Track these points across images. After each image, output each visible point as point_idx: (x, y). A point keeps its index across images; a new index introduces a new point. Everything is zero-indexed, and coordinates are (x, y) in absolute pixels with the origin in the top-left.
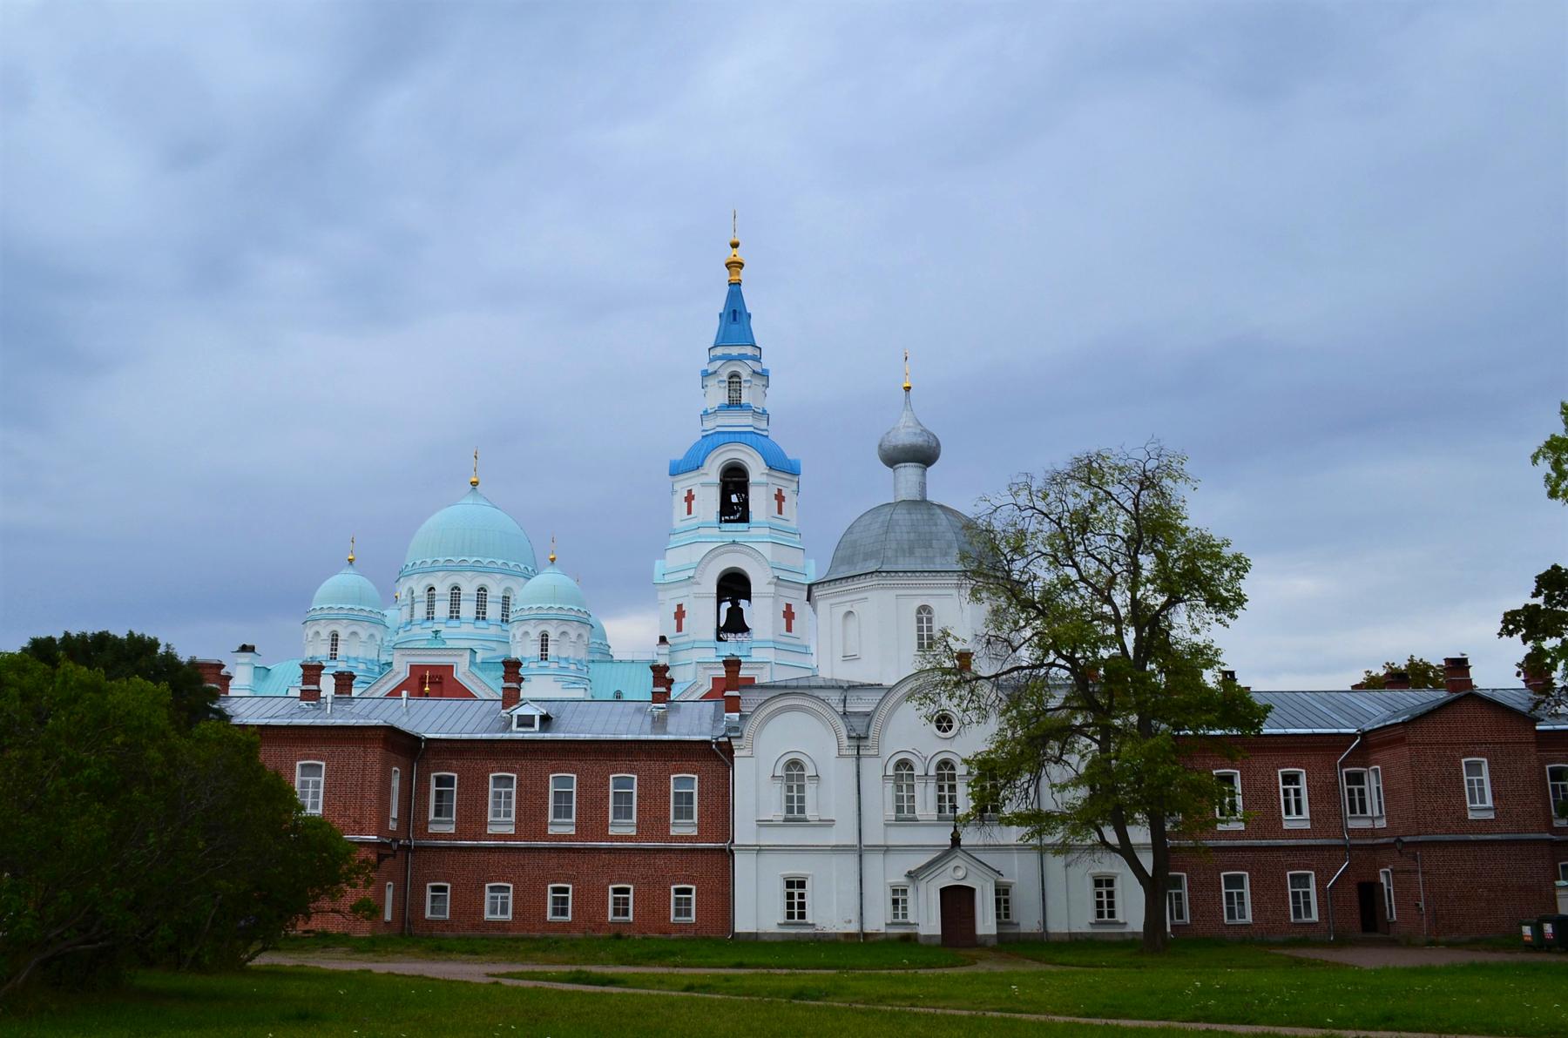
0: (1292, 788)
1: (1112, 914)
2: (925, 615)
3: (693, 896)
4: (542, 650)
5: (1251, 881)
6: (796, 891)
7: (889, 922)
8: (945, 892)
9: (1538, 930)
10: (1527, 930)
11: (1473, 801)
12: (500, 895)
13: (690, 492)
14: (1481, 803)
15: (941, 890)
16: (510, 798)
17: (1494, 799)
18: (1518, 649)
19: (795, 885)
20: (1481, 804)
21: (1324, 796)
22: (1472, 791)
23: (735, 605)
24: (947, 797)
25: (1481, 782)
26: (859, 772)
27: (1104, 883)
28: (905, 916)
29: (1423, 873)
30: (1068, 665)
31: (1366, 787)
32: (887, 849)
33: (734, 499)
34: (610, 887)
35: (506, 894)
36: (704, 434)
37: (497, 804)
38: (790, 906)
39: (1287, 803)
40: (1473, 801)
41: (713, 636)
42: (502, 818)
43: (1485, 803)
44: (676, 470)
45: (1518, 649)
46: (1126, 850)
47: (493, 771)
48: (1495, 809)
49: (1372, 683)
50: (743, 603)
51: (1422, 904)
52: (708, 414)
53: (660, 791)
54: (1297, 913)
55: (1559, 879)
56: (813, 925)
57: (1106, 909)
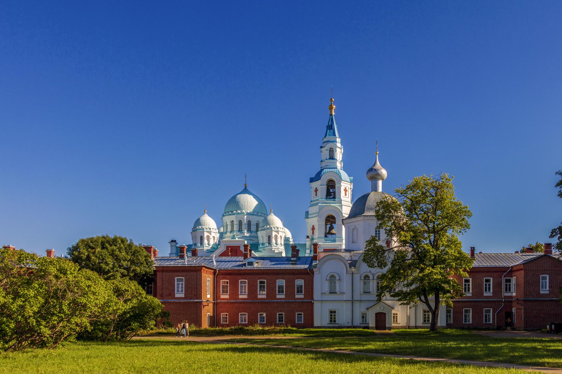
1: (397, 321)
3: (303, 316)
5: (472, 311)
6: (333, 314)
7: (361, 323)
8: (377, 314)
10: (548, 327)
11: (542, 288)
12: (244, 316)
13: (316, 188)
14: (545, 289)
15: (376, 314)
16: (246, 287)
17: (549, 287)
19: (332, 313)
20: (545, 290)
21: (498, 286)
22: (542, 285)
23: (332, 225)
25: (546, 282)
28: (366, 321)
29: (524, 309)
31: (511, 283)
32: (361, 301)
33: (331, 191)
34: (277, 313)
35: (246, 316)
36: (322, 168)
37: (241, 289)
39: (486, 288)
40: (542, 288)
41: (323, 236)
42: (243, 293)
44: (312, 180)
47: (240, 279)
48: (549, 290)
51: (523, 319)
53: (292, 284)
54: (486, 321)
56: (338, 324)
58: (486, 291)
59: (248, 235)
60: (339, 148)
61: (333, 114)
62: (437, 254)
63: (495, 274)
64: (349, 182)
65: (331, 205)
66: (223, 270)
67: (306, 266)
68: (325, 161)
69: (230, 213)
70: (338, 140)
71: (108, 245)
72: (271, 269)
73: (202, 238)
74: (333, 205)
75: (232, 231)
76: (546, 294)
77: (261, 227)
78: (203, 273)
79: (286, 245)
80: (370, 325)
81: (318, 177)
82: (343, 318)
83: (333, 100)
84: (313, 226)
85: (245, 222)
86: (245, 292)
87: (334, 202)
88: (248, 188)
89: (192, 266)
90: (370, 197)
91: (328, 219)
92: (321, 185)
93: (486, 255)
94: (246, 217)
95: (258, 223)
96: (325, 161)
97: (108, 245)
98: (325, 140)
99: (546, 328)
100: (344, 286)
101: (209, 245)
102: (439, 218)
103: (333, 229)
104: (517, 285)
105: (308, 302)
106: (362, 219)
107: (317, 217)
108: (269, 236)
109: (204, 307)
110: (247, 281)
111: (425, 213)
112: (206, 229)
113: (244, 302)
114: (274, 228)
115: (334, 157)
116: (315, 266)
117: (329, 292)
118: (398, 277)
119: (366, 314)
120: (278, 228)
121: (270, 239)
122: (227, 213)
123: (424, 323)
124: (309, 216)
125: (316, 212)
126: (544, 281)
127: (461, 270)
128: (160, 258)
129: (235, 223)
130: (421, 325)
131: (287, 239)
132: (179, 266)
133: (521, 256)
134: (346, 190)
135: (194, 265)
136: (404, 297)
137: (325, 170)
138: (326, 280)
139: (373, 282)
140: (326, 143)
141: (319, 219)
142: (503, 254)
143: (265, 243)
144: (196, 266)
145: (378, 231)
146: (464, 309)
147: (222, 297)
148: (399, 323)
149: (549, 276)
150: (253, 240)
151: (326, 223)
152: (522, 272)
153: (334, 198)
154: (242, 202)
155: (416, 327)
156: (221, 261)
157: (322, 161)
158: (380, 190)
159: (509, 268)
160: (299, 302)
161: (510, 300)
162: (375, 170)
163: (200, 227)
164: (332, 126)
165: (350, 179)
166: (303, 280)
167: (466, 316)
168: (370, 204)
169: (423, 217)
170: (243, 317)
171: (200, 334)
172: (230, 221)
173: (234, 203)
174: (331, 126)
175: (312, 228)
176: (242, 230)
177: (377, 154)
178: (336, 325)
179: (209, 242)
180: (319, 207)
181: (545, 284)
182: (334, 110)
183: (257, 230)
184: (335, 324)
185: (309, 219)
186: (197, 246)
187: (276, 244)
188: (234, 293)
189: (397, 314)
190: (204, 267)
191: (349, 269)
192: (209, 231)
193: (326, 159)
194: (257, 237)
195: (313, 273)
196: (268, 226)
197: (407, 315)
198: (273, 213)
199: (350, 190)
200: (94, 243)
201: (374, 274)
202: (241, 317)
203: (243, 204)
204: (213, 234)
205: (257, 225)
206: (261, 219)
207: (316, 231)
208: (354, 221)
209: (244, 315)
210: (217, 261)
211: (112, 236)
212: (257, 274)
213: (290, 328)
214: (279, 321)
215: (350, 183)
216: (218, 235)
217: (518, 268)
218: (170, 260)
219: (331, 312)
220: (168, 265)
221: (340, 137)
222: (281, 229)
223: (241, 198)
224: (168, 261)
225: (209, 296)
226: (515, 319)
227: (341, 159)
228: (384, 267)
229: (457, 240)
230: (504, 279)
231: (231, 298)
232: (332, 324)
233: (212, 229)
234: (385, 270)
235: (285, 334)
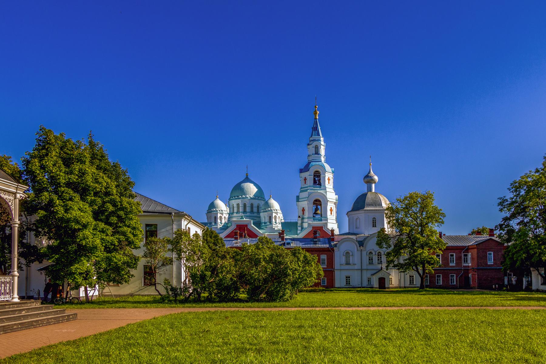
0: (452, 257)
2: (374, 220)
6: (348, 279)
10: (494, 286)
11: (489, 260)
13: (305, 178)
15: (379, 278)
17: (494, 260)
19: (348, 278)
20: (491, 262)
21: (459, 259)
22: (489, 259)
25: (491, 257)
28: (370, 283)
29: (477, 275)
33: (316, 179)
38: (347, 282)
39: (451, 260)
40: (489, 260)
44: (301, 171)
46: (417, 271)
54: (451, 282)
57: (412, 282)
58: (451, 262)
60: (323, 145)
61: (317, 117)
63: (457, 251)
67: (328, 246)
69: (236, 197)
70: (322, 139)
73: (216, 218)
74: (319, 191)
76: (491, 265)
77: (263, 209)
80: (375, 286)
81: (306, 169)
88: (249, 177)
91: (315, 202)
93: (449, 237)
98: (311, 139)
100: (355, 259)
101: (221, 224)
104: (472, 258)
105: (330, 271)
112: (219, 211)
114: (274, 210)
116: (336, 245)
119: (370, 279)
124: (300, 200)
129: (240, 205)
130: (408, 286)
134: (329, 179)
136: (401, 267)
137: (313, 163)
152: (476, 250)
155: (405, 287)
157: (309, 156)
161: (467, 268)
162: (370, 176)
163: (215, 209)
168: (369, 201)
169: (414, 216)
173: (238, 190)
186: (212, 225)
187: (276, 223)
191: (359, 248)
192: (222, 212)
193: (313, 154)
194: (260, 217)
195: (333, 251)
196: (270, 209)
199: (332, 179)
203: (247, 190)
204: (224, 215)
205: (258, 207)
206: (262, 203)
216: (228, 215)
217: (473, 247)
221: (323, 136)
227: (324, 154)
233: (223, 211)
234: (389, 250)
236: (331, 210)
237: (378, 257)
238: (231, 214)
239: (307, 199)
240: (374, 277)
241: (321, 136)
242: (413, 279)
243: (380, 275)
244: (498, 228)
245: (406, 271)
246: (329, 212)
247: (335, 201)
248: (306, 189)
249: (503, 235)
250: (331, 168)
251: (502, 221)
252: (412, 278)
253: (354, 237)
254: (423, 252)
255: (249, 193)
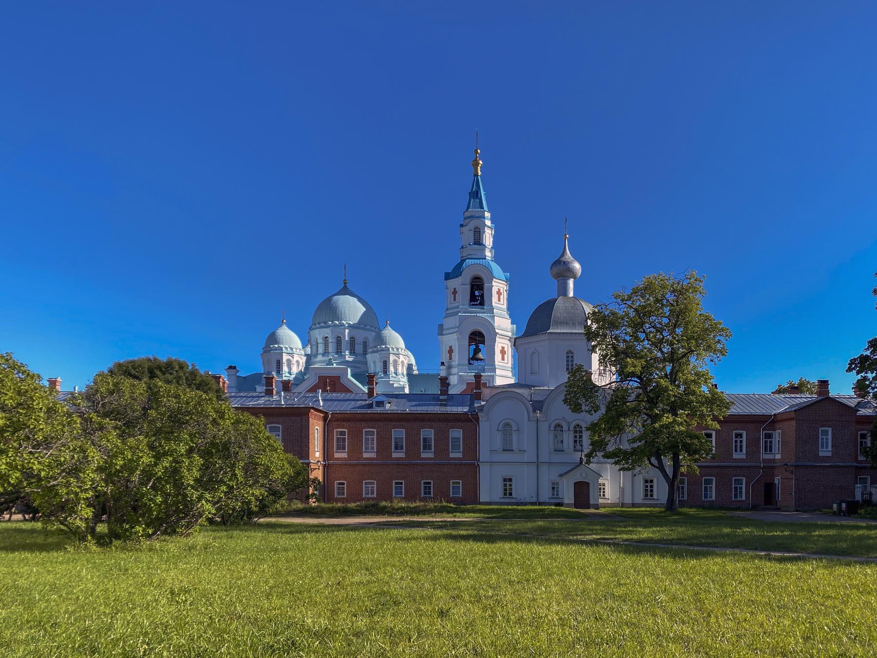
0: (739, 440)
2: (570, 355)
3: (461, 485)
4: (384, 369)
6: (508, 483)
9: (840, 505)
10: (835, 506)
11: (822, 447)
12: (370, 486)
18: (854, 377)
19: (507, 480)
20: (825, 451)
21: (753, 443)
23: (477, 346)
24: (578, 441)
25: (827, 439)
26: (537, 429)
27: (648, 482)
28: (557, 495)
30: (638, 381)
31: (773, 440)
33: (477, 293)
37: (367, 444)
38: (506, 490)
39: (736, 446)
40: (822, 447)
41: (467, 362)
42: (370, 450)
43: (504, 360)
44: (448, 277)
45: (854, 377)
46: (661, 468)
49: (780, 391)
50: (481, 346)
51: (793, 494)
52: (463, 248)
54: (736, 496)
55: (857, 484)
57: (649, 493)
58: (736, 451)
59: (351, 359)
60: (488, 227)
61: (480, 173)
62: (678, 394)
64: (505, 281)
65: (478, 315)
66: (339, 413)
67: (466, 409)
68: (467, 247)
69: (323, 324)
70: (487, 215)
71: (158, 373)
72: (413, 413)
73: (279, 364)
75: (326, 352)
76: (827, 457)
77: (372, 348)
78: (310, 419)
79: (410, 375)
80: (566, 501)
81: (456, 272)
82: (523, 490)
83: (479, 151)
84: (451, 347)
85: (347, 339)
86: (372, 448)
87: (482, 311)
89: (295, 408)
90: (558, 305)
91: (472, 336)
92: (462, 285)
93: (732, 396)
94: (347, 331)
95: (365, 341)
96: (467, 247)
97: (159, 373)
98: (467, 214)
99: (831, 508)
101: (290, 374)
102: (683, 340)
103: (480, 353)
104: (784, 443)
106: (547, 338)
107: (458, 333)
108: (277, 361)
109: (313, 471)
110: (375, 430)
111: (658, 331)
112: (286, 348)
113: (370, 463)
114: (393, 349)
115: (481, 242)
116: (481, 408)
117: (502, 450)
118: (618, 427)
119: (558, 484)
120: (398, 349)
121: (386, 366)
122: (317, 325)
123: (645, 499)
124: (444, 332)
125: (455, 326)
126: (825, 437)
127: (709, 419)
128: (233, 394)
129: (330, 340)
131: (410, 367)
132: (261, 408)
133: (784, 398)
134: (499, 293)
135: (298, 406)
136: (620, 457)
138: (498, 430)
139: (569, 434)
140: (468, 219)
141: (460, 336)
142: (757, 396)
143: (379, 373)
144: (300, 407)
145: (571, 356)
146: (703, 478)
147: (337, 455)
148: (514, 497)
149: (832, 430)
150: (360, 368)
151: (469, 343)
152: (793, 423)
153: (482, 304)
154: (340, 308)
155: (633, 505)
156: (331, 400)
157: (462, 247)
158: (571, 294)
159: (771, 416)
160: (455, 465)
162: (564, 262)
163: (276, 346)
164: (477, 192)
165: (505, 276)
166: (461, 430)
167: (706, 488)
170: (370, 489)
171: (313, 513)
172: (322, 337)
174: (475, 192)
175: (448, 351)
176: (341, 352)
177: (565, 239)
178: (514, 501)
179: (291, 370)
180: (459, 317)
181: (826, 442)
182: (481, 167)
183: (365, 353)
184: (511, 498)
185: (444, 336)
187: (396, 373)
188: (356, 450)
189: (604, 484)
190: (313, 408)
191: (532, 414)
193: (470, 244)
194: (366, 363)
195: (477, 420)
196: (384, 346)
197: (620, 486)
198: (391, 327)
199: (505, 292)
200: (137, 370)
201: (569, 423)
202: (366, 487)
204: (296, 358)
205: (365, 344)
206: (371, 336)
207: (455, 355)
208: (527, 341)
209: (371, 483)
210: (323, 400)
211: (163, 359)
212: (390, 420)
213: (445, 504)
214: (425, 493)
215: (506, 282)
216: (304, 359)
218: (249, 397)
219: (505, 480)
220: (255, 405)
222: (403, 351)
223: (340, 301)
224: (253, 398)
225: (317, 454)
226: (778, 494)
228: (595, 413)
229: (707, 373)
230: (763, 433)
231: (350, 457)
232: (554, 498)
233: (294, 350)
234: (595, 417)
235: (455, 514)
236: (503, 352)
237: (575, 437)
238: (309, 358)
239: (456, 330)
240: (564, 479)
241: (486, 208)
242: (651, 486)
243: (578, 476)
244: (856, 366)
245: (633, 468)
246: (498, 356)
247: (510, 334)
248: (456, 310)
249: (871, 383)
250: (504, 272)
251: (868, 349)
252: (649, 484)
253: (524, 392)
254: (674, 420)
255: (348, 317)
